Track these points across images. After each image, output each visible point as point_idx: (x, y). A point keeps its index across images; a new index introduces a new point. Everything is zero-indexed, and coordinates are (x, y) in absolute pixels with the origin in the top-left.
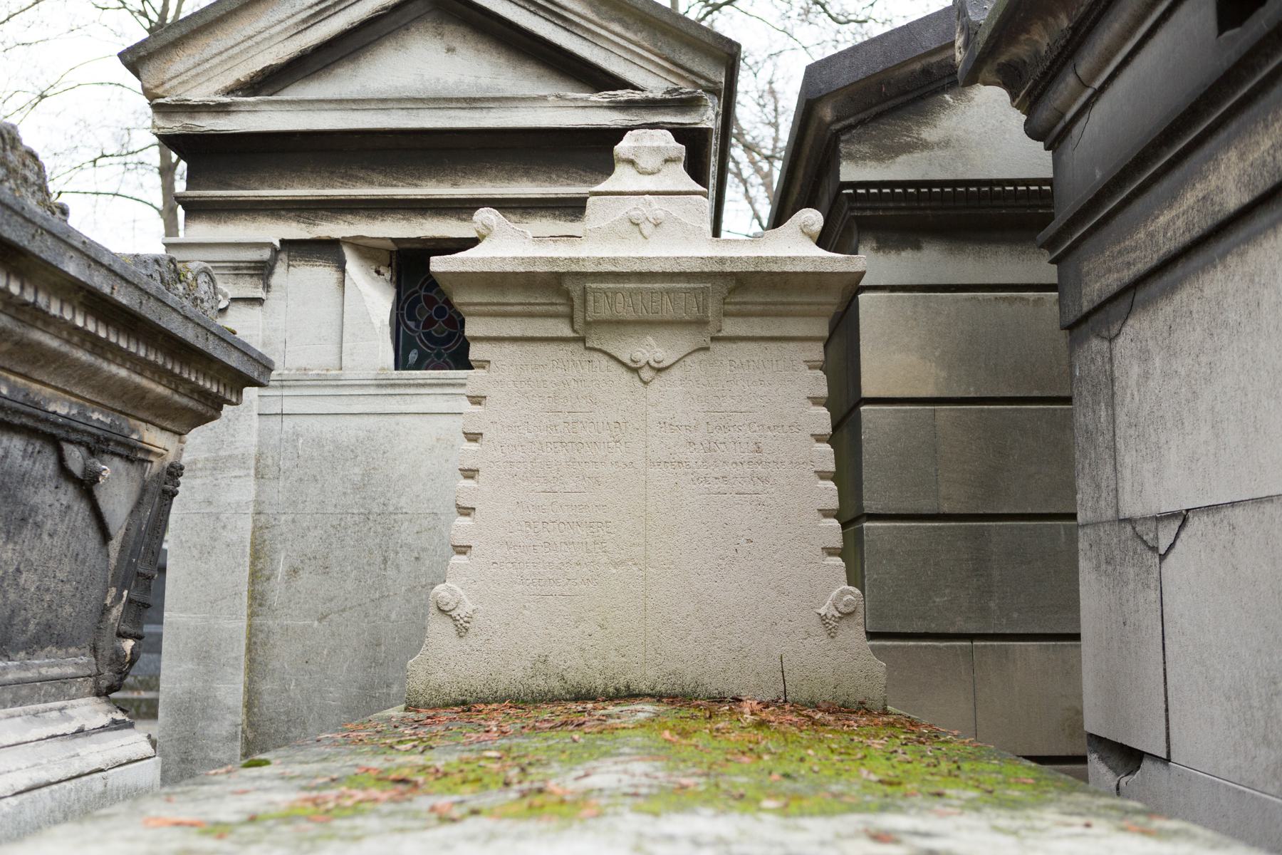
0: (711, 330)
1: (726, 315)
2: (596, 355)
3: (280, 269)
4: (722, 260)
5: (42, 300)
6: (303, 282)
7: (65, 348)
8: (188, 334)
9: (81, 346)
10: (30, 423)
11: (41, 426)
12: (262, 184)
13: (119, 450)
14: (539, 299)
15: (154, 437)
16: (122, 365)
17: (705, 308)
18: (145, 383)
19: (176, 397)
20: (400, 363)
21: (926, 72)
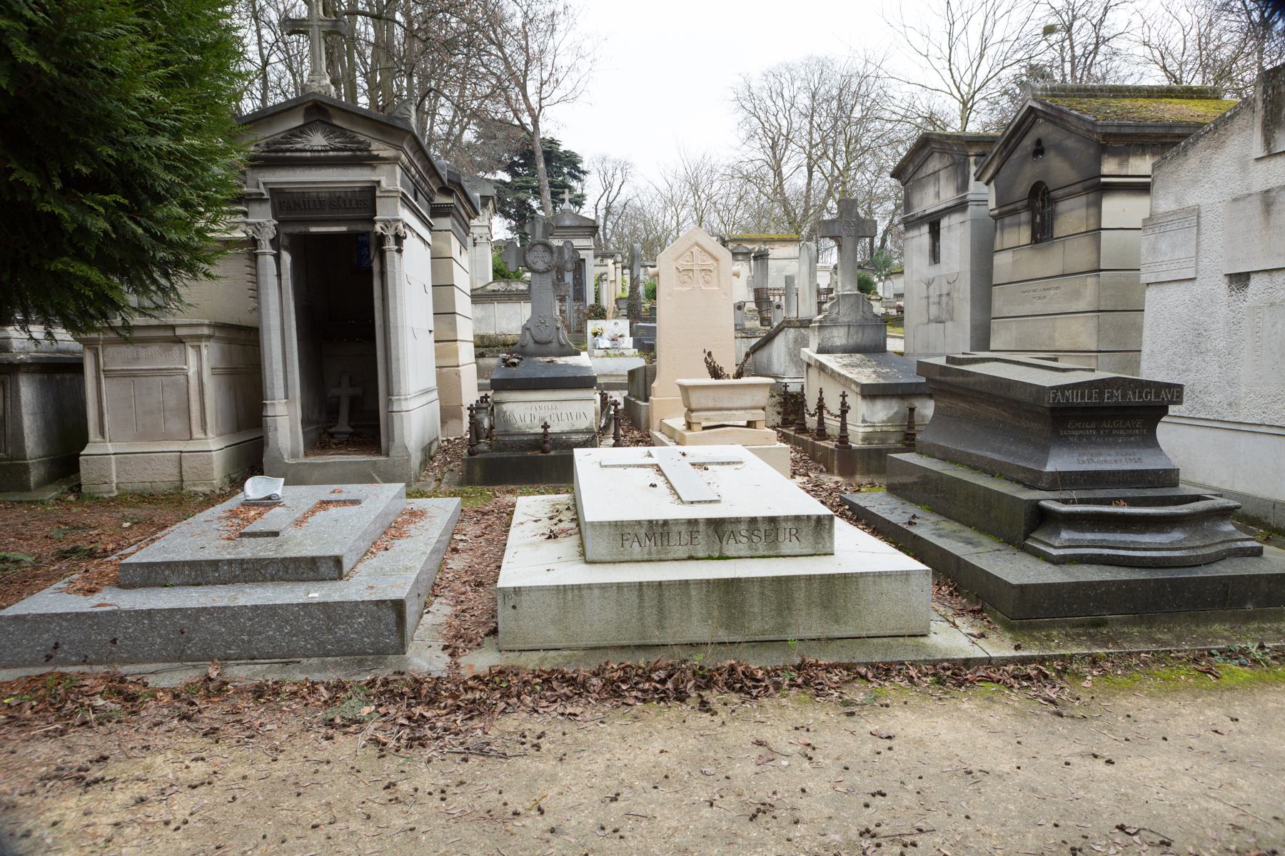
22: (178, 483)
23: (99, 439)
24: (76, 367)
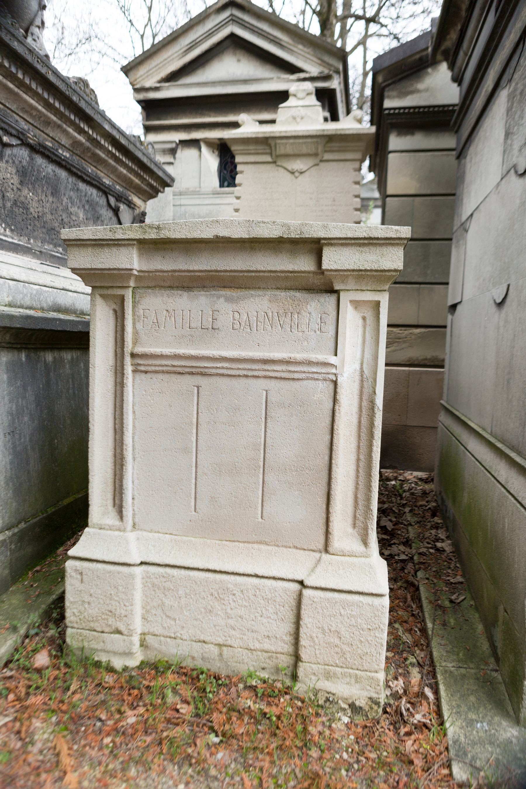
0: (320, 157)
1: (326, 151)
2: (280, 168)
3: (179, 151)
4: (324, 130)
5: (99, 138)
6: (187, 155)
7: (106, 158)
8: (145, 160)
9: (111, 158)
10: (98, 184)
11: (101, 186)
12: (172, 118)
13: (125, 202)
14: (260, 147)
15: (136, 200)
16: (124, 168)
17: (317, 149)
18: (132, 177)
19: (142, 185)
20: (222, 185)
21: (421, 59)
22: (285, 661)
23: (112, 519)
24: (74, 339)
